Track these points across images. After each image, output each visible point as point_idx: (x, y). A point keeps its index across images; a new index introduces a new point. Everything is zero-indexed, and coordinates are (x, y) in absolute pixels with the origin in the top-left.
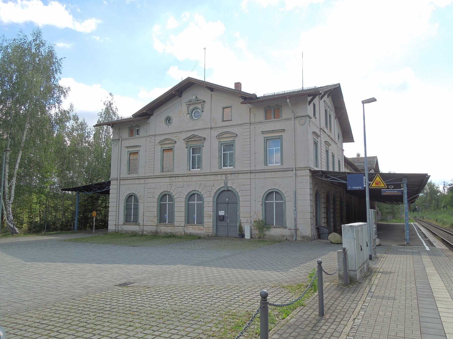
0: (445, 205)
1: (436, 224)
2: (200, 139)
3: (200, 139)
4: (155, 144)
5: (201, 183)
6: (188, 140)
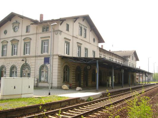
6: (12, 41)
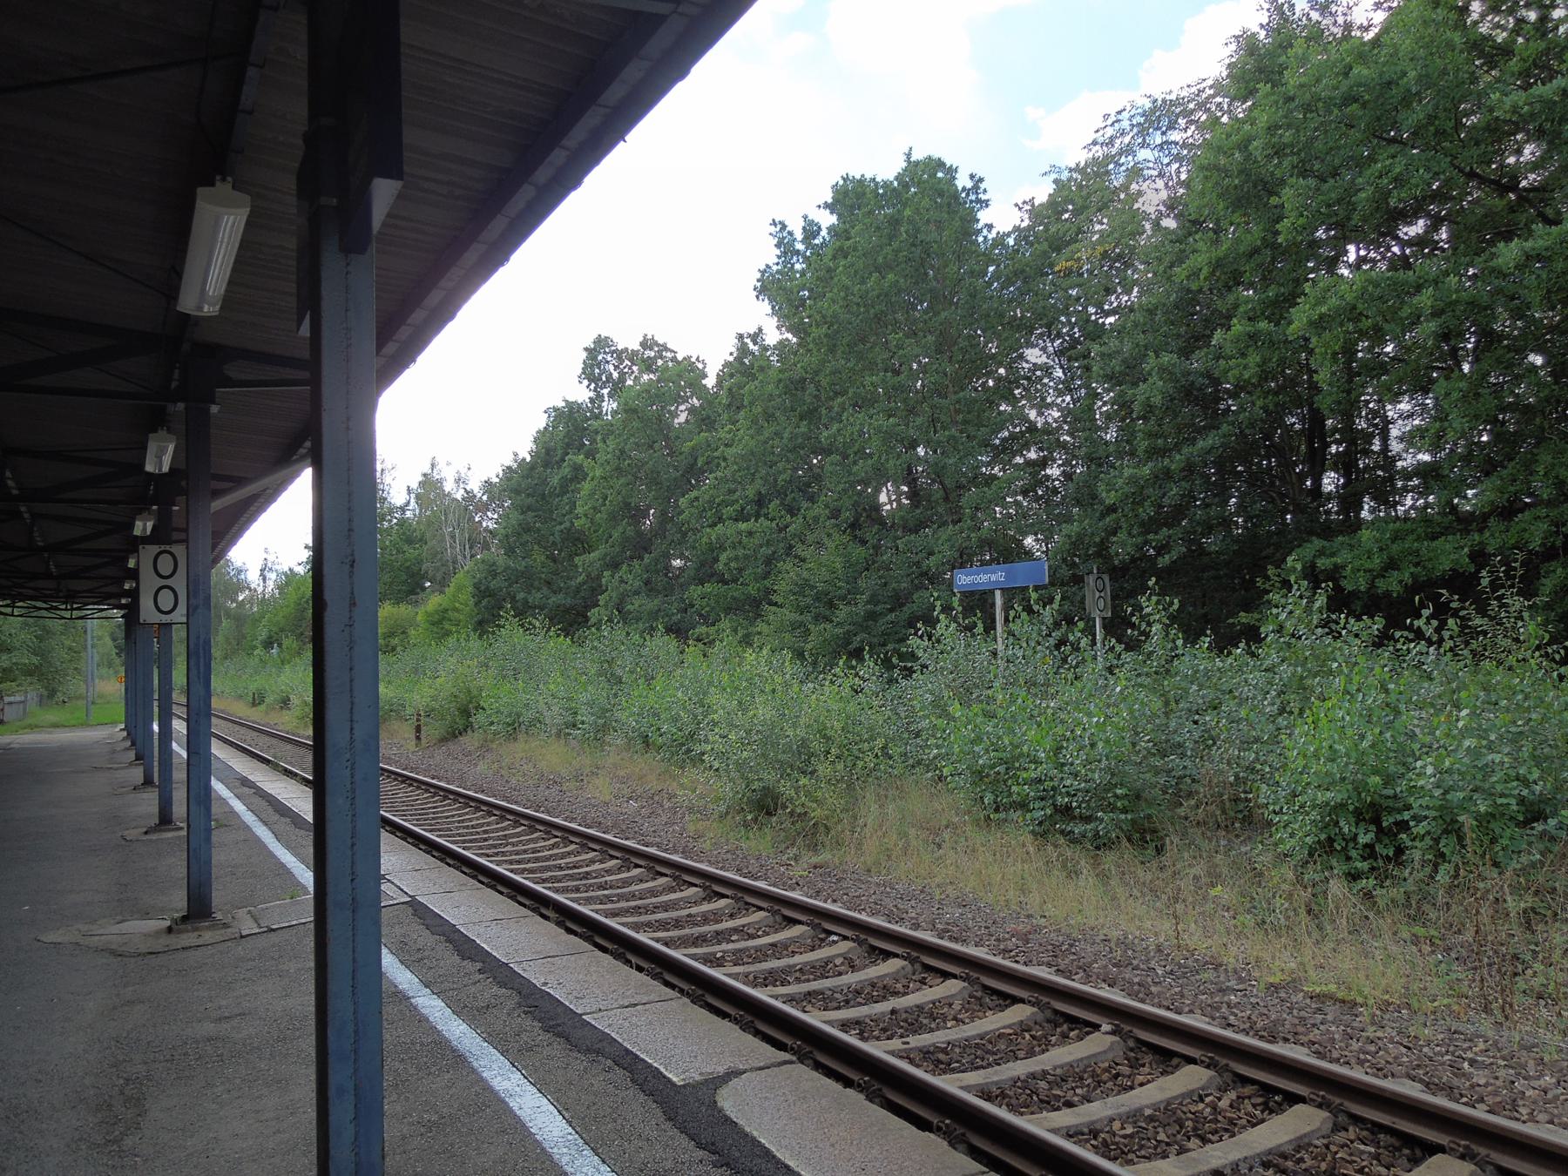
0: (270, 637)
1: (254, 715)
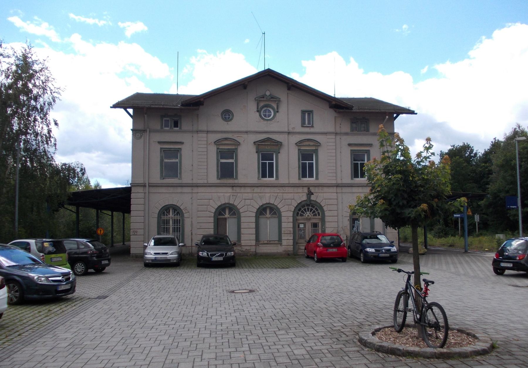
2: (277, 144)
3: (277, 144)
4: (207, 142)
5: (277, 195)
